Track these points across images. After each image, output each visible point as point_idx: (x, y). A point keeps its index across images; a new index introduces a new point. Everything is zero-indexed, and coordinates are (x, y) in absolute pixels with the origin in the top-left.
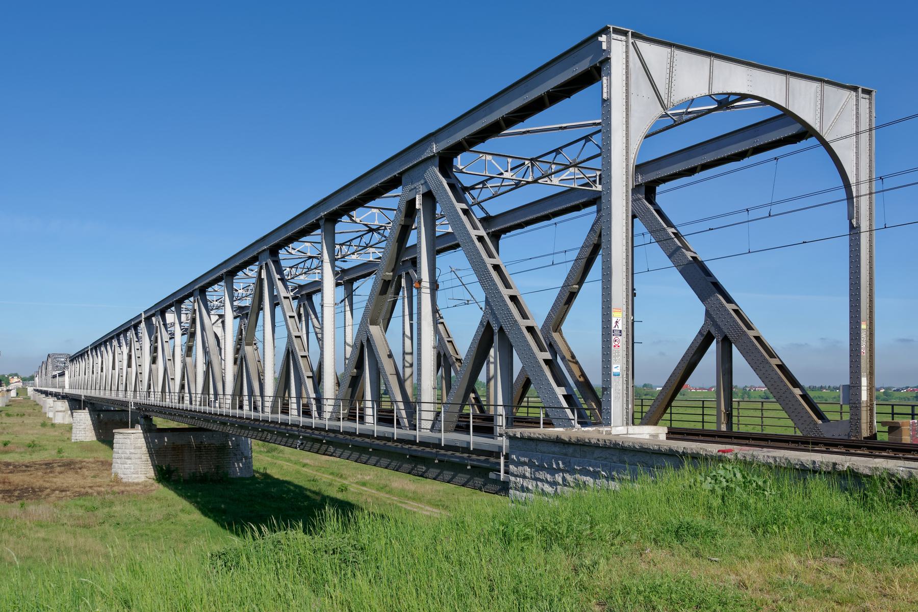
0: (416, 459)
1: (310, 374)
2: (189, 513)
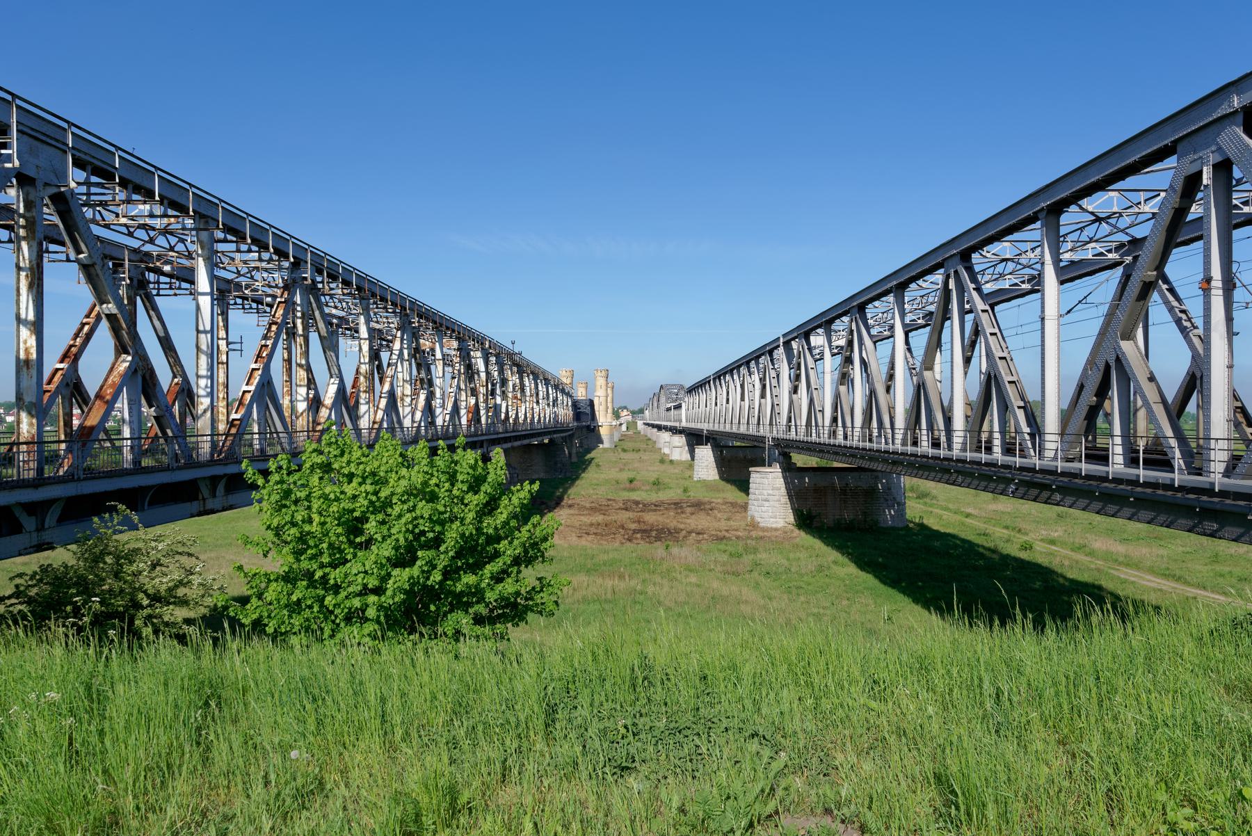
0: (1209, 513)
1: (1022, 404)
2: (843, 566)
